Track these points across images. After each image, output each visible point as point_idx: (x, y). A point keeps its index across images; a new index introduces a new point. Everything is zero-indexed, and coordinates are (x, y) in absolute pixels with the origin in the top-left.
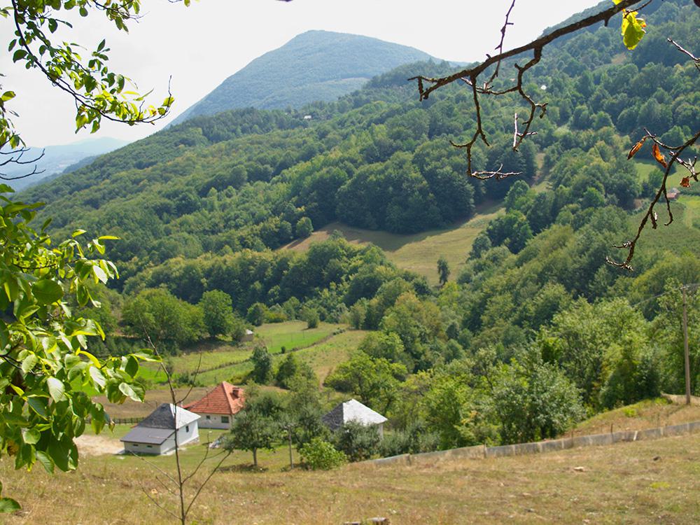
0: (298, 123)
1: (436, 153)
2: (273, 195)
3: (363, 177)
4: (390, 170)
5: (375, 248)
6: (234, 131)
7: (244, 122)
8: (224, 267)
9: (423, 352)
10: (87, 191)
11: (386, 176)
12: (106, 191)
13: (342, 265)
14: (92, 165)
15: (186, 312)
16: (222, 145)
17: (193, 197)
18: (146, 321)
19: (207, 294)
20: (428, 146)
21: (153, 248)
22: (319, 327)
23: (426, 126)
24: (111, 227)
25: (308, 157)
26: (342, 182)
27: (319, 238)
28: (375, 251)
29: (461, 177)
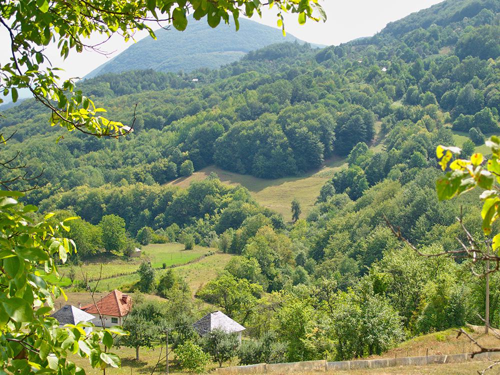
1: (296, 116)
3: (237, 131)
5: (243, 189)
6: (135, 87)
7: (145, 80)
8: (121, 196)
10: (14, 127)
12: (29, 128)
14: (19, 107)
16: (125, 97)
21: (64, 177)
25: (193, 112)
26: (219, 134)
27: (198, 178)
28: (243, 191)
29: (314, 136)
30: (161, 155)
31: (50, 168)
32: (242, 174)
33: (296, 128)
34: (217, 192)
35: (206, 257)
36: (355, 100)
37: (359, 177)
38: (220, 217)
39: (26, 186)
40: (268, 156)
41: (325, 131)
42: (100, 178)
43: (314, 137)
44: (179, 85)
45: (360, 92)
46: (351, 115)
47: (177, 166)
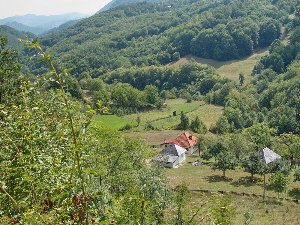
0: (166, 9)
1: (237, 25)
2: (161, 41)
3: (204, 35)
4: (216, 32)
5: (211, 67)
6: (138, 12)
7: (142, 8)
8: (143, 73)
9: (248, 117)
10: (75, 36)
11: (214, 35)
12: (84, 36)
13: (196, 74)
14: (76, 25)
15: (140, 94)
16: (134, 18)
17: (124, 41)
18: (123, 98)
19: (147, 87)
20: (233, 22)
21: (110, 63)
22: (192, 102)
23: (230, 12)
24: (91, 53)
25: (175, 25)
26: (193, 37)
27: (183, 62)
28: (212, 68)
29: (248, 36)
30: (160, 49)
31: (102, 58)
32: (207, 59)
33: (237, 32)
34: (197, 70)
35: (201, 107)
36: (268, 15)
37: (278, 60)
38: (200, 83)
39: (89, 68)
40: (222, 48)
41: (254, 33)
42: (128, 63)
43: (248, 37)
44: (161, 9)
45: (270, 10)
46: (268, 24)
47: (171, 55)
